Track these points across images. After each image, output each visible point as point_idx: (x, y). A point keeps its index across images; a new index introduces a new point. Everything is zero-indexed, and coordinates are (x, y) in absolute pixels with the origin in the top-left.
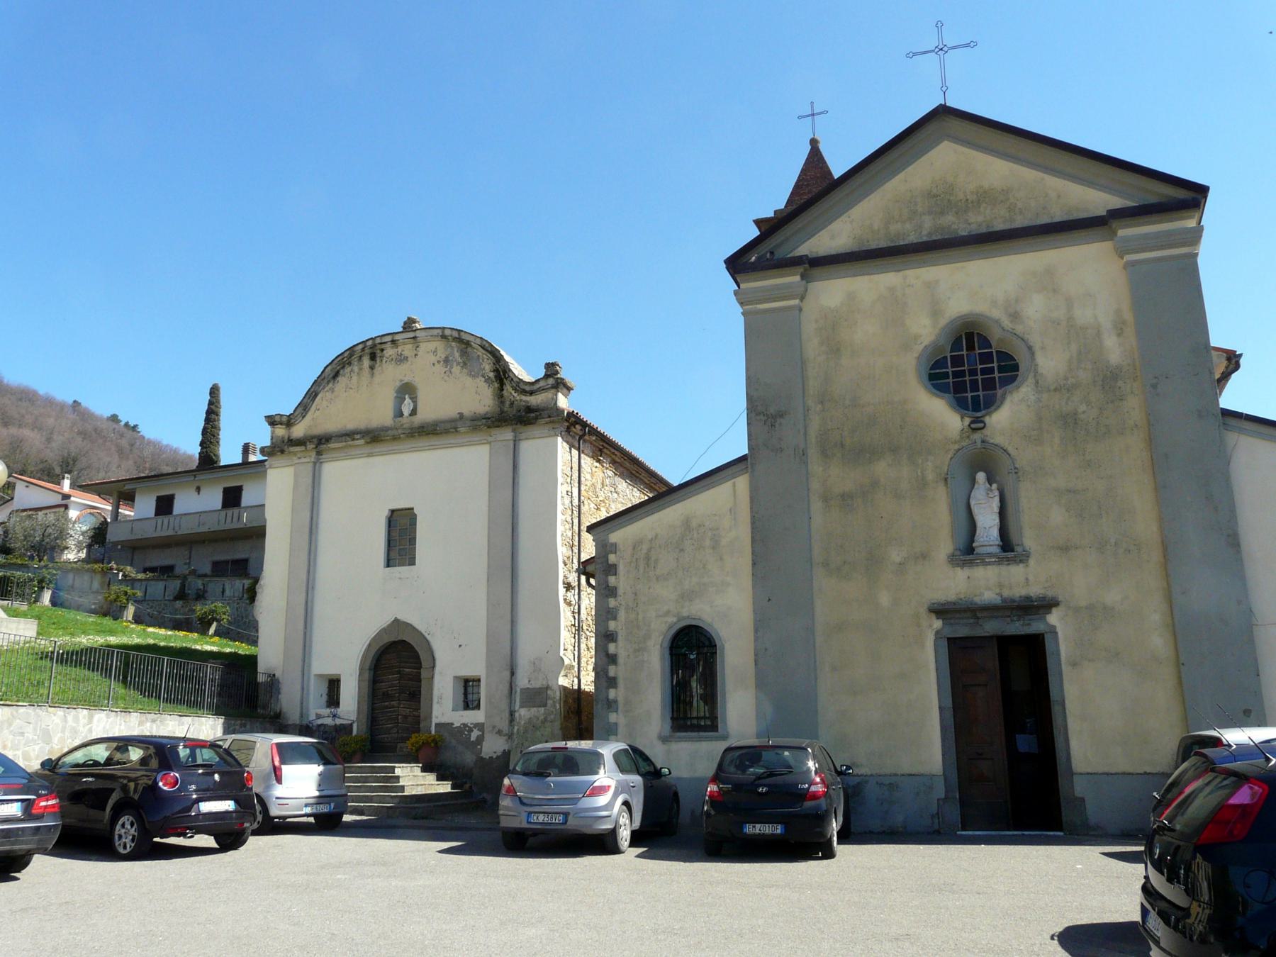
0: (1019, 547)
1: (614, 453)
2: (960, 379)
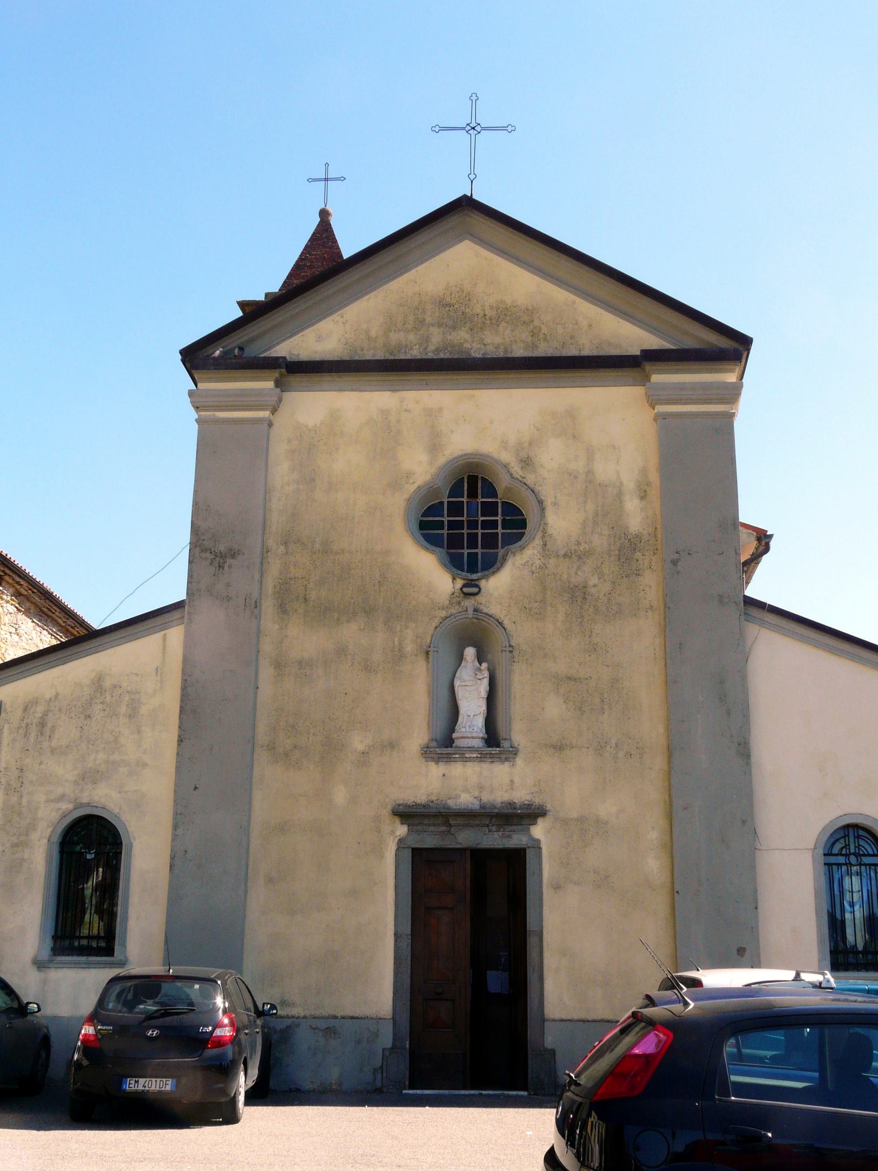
0: (506, 741)
1: (18, 583)
2: (458, 531)
